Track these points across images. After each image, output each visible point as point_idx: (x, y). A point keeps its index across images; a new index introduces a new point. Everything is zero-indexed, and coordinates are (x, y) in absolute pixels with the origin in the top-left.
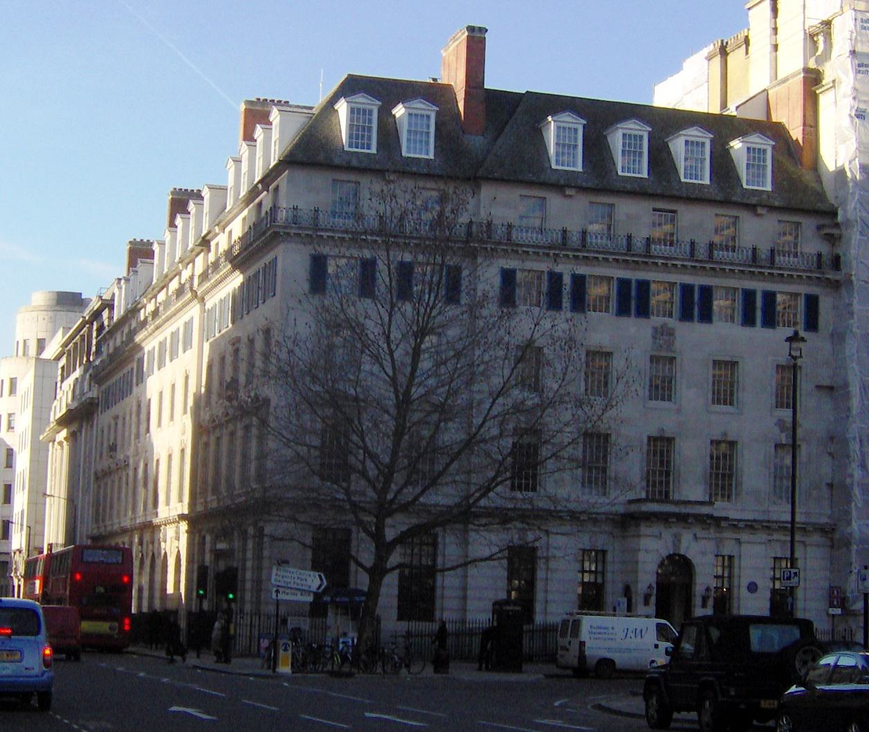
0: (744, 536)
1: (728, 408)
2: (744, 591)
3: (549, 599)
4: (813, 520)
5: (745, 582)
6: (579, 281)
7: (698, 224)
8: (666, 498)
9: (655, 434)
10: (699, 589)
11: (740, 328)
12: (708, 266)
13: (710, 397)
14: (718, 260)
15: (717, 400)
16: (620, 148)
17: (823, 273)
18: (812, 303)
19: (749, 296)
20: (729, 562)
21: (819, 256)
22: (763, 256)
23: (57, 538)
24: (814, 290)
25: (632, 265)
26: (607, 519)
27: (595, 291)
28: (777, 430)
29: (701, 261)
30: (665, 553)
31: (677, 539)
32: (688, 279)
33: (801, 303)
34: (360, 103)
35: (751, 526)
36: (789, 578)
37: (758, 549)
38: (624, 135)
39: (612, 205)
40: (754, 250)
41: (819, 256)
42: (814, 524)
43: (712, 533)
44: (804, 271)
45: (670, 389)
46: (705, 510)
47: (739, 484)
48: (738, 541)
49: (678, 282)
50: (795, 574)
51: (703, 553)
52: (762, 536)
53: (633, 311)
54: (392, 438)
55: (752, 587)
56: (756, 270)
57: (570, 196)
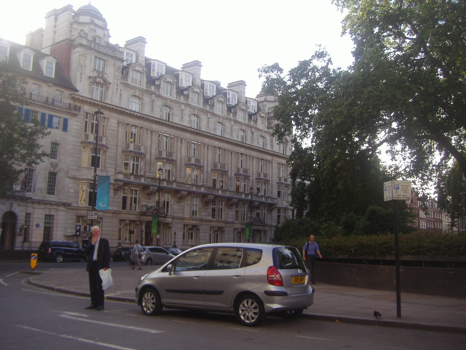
0: (36, 206)
2: (34, 228)
3: (176, 241)
4: (60, 201)
5: (35, 224)
10: (19, 226)
12: (51, 107)
14: (33, 99)
16: (45, 66)
17: (71, 111)
18: (66, 121)
20: (28, 215)
21: (70, 104)
22: (50, 101)
24: (66, 116)
26: (62, 204)
27: (55, 120)
28: (50, 166)
30: (6, 211)
31: (11, 205)
33: (62, 121)
34: (49, 60)
39: (40, 86)
40: (47, 98)
41: (70, 104)
42: (61, 203)
43: (24, 204)
44: (64, 109)
46: (22, 194)
48: (34, 208)
49: (63, 117)
51: (22, 212)
52: (42, 206)
54: (359, 216)
55: (38, 226)
56: (54, 108)
57: (50, 86)
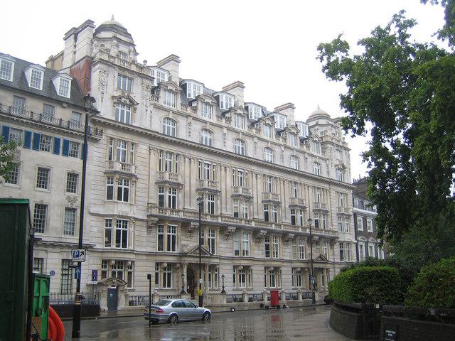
1: (44, 190)
6: (66, 143)
7: (35, 108)
8: (107, 220)
9: (39, 203)
11: (63, 157)
13: (36, 184)
15: (39, 186)
19: (28, 134)
23: (53, 302)
25: (30, 125)
29: (36, 121)
32: (29, 129)
35: (53, 245)
36: (78, 256)
37: (56, 255)
38: (33, 71)
45: (16, 178)
47: (48, 225)
50: (83, 253)
52: (58, 250)
53: (31, 147)
